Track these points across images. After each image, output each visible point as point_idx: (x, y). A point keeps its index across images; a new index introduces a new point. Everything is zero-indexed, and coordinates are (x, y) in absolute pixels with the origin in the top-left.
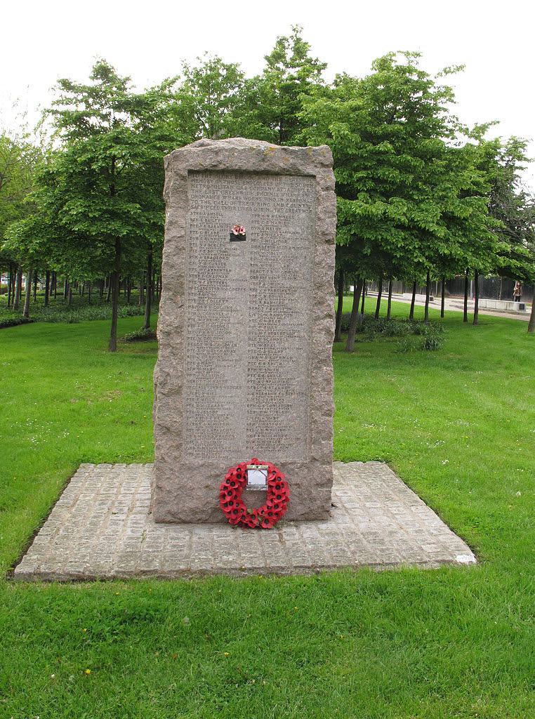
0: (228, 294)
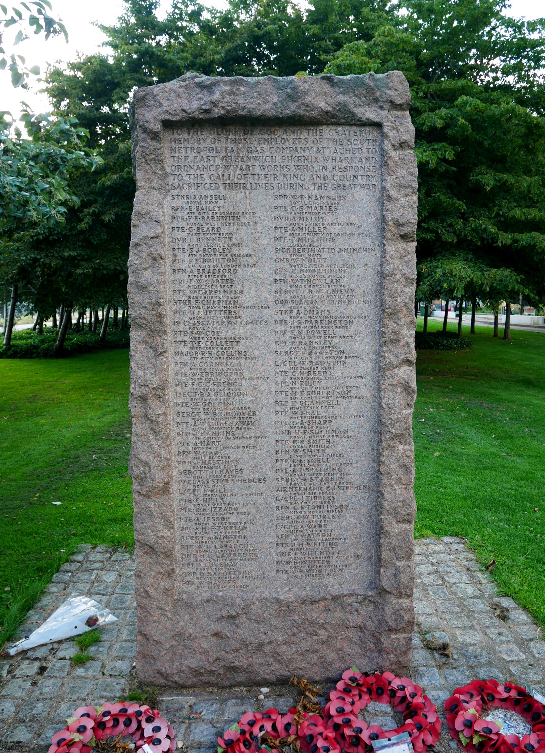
0: (240, 330)
